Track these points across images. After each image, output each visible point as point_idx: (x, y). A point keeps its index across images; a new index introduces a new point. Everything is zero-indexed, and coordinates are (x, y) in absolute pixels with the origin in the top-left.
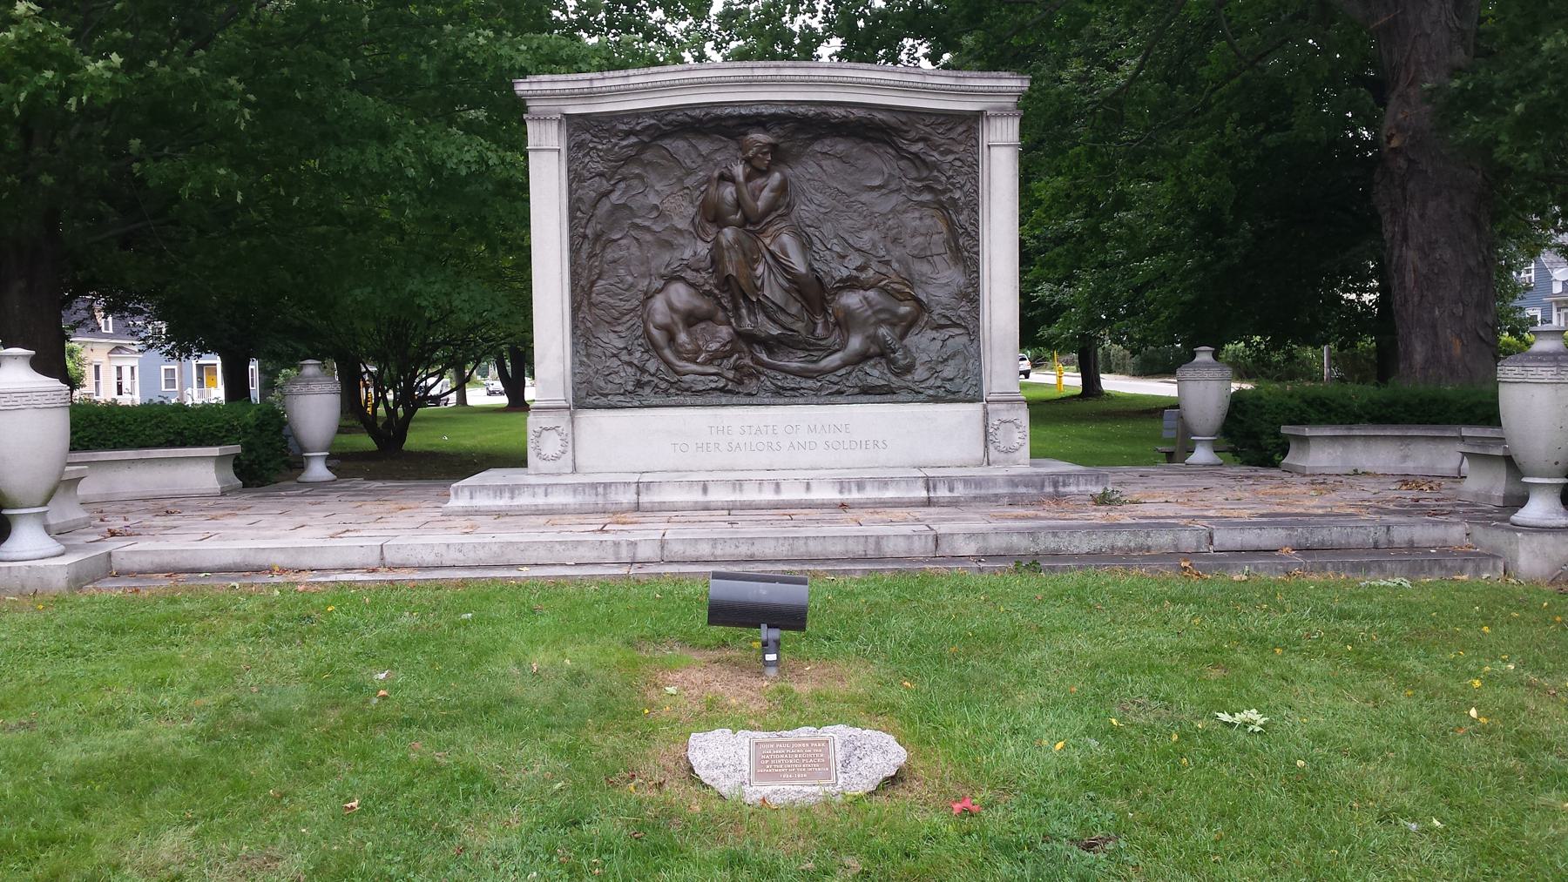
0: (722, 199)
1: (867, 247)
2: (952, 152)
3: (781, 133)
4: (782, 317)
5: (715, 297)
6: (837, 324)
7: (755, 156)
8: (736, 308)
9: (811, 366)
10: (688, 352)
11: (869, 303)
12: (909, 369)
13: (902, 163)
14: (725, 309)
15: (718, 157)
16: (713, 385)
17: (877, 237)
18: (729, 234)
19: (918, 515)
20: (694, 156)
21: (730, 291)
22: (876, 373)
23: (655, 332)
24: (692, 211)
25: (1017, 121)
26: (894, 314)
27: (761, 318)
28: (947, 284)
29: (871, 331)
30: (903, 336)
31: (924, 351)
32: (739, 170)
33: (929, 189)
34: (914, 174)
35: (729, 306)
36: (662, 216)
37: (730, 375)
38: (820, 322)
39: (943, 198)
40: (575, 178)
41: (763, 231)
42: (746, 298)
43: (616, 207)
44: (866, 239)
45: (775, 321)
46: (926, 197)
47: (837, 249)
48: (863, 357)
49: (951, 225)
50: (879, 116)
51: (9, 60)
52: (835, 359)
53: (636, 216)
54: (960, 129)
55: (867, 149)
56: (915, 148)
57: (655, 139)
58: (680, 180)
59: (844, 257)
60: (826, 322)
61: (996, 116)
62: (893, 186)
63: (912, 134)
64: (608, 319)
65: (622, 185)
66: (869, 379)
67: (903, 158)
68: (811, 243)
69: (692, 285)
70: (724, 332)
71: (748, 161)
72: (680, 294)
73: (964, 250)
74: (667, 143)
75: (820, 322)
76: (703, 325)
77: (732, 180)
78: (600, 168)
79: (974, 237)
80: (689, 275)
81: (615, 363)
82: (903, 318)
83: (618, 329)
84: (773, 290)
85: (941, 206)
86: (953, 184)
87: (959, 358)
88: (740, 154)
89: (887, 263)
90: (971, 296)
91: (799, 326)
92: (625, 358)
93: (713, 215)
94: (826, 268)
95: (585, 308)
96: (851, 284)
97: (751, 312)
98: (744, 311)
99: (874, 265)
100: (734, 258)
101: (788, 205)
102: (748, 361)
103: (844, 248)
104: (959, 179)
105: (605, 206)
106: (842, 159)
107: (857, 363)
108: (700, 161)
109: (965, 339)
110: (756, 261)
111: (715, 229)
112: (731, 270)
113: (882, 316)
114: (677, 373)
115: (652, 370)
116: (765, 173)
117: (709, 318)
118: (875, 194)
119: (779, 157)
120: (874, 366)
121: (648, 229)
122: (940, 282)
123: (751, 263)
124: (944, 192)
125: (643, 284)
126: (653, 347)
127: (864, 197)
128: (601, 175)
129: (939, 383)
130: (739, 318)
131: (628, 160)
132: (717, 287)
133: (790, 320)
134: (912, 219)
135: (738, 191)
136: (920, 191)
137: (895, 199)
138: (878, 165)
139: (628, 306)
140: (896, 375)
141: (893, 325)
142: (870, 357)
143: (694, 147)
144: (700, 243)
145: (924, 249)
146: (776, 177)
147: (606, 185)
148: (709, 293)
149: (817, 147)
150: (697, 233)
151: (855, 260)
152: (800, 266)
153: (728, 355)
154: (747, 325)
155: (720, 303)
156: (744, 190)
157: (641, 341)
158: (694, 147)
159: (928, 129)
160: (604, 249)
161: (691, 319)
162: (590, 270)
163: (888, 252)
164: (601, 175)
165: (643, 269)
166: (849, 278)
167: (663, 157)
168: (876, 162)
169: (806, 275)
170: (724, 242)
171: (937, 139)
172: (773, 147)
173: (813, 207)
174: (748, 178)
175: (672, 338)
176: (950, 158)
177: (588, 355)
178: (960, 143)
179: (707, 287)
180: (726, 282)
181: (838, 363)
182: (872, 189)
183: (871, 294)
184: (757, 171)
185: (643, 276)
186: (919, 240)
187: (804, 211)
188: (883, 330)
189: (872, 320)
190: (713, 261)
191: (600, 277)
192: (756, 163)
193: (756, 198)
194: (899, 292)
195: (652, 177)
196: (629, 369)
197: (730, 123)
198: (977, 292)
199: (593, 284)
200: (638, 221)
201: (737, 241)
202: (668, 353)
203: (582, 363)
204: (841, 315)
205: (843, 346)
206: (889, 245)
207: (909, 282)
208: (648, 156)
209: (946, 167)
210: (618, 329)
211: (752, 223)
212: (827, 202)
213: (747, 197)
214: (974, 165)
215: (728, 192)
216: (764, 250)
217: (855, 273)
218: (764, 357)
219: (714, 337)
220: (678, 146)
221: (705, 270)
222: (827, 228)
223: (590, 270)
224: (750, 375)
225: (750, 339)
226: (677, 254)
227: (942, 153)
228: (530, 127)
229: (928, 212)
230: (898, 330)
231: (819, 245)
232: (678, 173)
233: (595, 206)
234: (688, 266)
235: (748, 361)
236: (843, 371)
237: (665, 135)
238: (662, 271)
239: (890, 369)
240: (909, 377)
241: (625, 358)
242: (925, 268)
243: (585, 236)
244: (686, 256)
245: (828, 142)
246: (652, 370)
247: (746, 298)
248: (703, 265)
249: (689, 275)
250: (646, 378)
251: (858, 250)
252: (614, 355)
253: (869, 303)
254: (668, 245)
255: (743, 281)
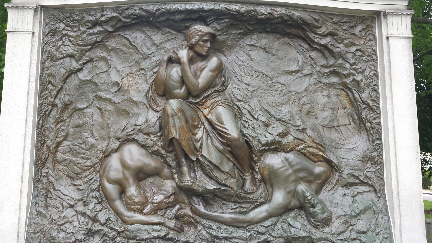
0: (169, 76)
1: (286, 118)
2: (354, 45)
3: (218, 27)
4: (218, 175)
5: (162, 156)
6: (263, 180)
7: (197, 43)
8: (179, 165)
9: (241, 217)
10: (135, 203)
11: (290, 163)
12: (327, 222)
13: (314, 54)
14: (169, 166)
15: (168, 45)
16: (156, 234)
17: (295, 110)
18: (174, 104)
19: (153, 77)
20: (149, 44)
21: (176, 151)
22: (298, 225)
23: (109, 186)
24: (146, 87)
25: (409, 19)
26: (311, 173)
27: (199, 174)
28: (353, 149)
29: (292, 187)
30: (318, 191)
31: (337, 205)
32: (184, 54)
33: (335, 73)
34: (323, 62)
35: (173, 164)
36: (120, 89)
37: (172, 224)
38: (248, 178)
39: (348, 81)
40: (47, 58)
41: (202, 103)
42: (187, 157)
43: (84, 83)
44: (284, 112)
45: (211, 178)
46: (334, 80)
47: (262, 119)
48: (286, 210)
49: (353, 102)
50: (297, 14)
51: (126, 137)
52: (261, 211)
53: (100, 91)
54: (359, 28)
55: (286, 43)
56: (324, 41)
57: (117, 30)
58: (138, 62)
59: (267, 126)
60: (253, 179)
61: (392, 14)
62: (307, 71)
63: (323, 30)
64: (71, 175)
65: (90, 65)
66: (292, 230)
67: (315, 49)
68: (241, 114)
69: (143, 146)
70: (169, 186)
71: (191, 47)
72: (134, 155)
73: (367, 120)
74: (128, 34)
75: (248, 178)
76: (151, 180)
77: (178, 61)
78: (71, 50)
79: (375, 110)
80: (141, 137)
81: (69, 213)
82: (318, 176)
83: (78, 182)
84: (210, 151)
85: (346, 87)
86: (355, 70)
87: (370, 213)
88: (185, 43)
89: (303, 131)
90: (375, 158)
91: (231, 182)
92: (80, 208)
93: (163, 90)
94: (254, 134)
95: (49, 164)
96: (274, 147)
97: (191, 169)
98: (185, 169)
99: (293, 131)
100: (178, 123)
101: (223, 84)
102: (187, 211)
103: (268, 119)
104: (360, 65)
105: (74, 81)
106: (265, 50)
107: (280, 215)
108: (154, 49)
109: (372, 195)
110: (196, 127)
111: (164, 102)
112: (175, 134)
113: (301, 175)
114: (125, 222)
115: (103, 221)
116: (205, 57)
117: (156, 173)
118: (291, 77)
119: (216, 45)
120: (295, 218)
121: (110, 101)
122: (351, 149)
123: (192, 128)
124: (347, 76)
125: (102, 145)
126: (105, 199)
127: (283, 79)
128: (71, 56)
129: (354, 235)
130: (181, 174)
131: (94, 45)
132: (163, 147)
133: (224, 176)
134: (321, 98)
135: (183, 70)
136: (328, 75)
137: (306, 82)
138: (293, 56)
139: (88, 163)
140: (316, 227)
141: (310, 182)
142: (291, 210)
143: (150, 38)
144: (151, 113)
145: (332, 121)
146: (213, 62)
147: (75, 65)
148: (156, 153)
149: (248, 41)
150: (150, 106)
151: (278, 128)
152: (233, 132)
153: (170, 206)
154: (188, 180)
155: (166, 162)
156: (187, 68)
157: (96, 193)
158: (150, 38)
159: (335, 26)
160: (71, 115)
161: (141, 175)
162: (57, 133)
163: (303, 122)
164: (71, 56)
165: (103, 132)
166: (273, 142)
167: (125, 45)
168: (293, 53)
169: (238, 140)
170: (169, 111)
171: (342, 34)
172: (213, 37)
173: (243, 86)
174: (191, 61)
175: (123, 191)
176: (354, 49)
177: (47, 206)
178: (360, 38)
179: (155, 148)
180: (171, 144)
181: (264, 214)
182: (290, 73)
183: (291, 156)
184: (198, 56)
185: (103, 138)
186: (327, 113)
187: (236, 89)
188: (302, 187)
189: (292, 178)
190: (161, 128)
191: (66, 138)
192: (198, 49)
193: (197, 76)
194: (313, 154)
195: (114, 60)
196: (82, 219)
197: (177, 17)
198: (380, 156)
199: (59, 144)
200: (101, 94)
201: (181, 110)
202: (119, 204)
203: (39, 214)
204: (266, 173)
205: (268, 200)
206: (305, 118)
207: (321, 146)
208: (112, 43)
209: (349, 56)
210: (78, 182)
211: (194, 96)
212: (254, 82)
213: (190, 75)
214: (372, 57)
215: (175, 72)
216: (203, 119)
217: (278, 138)
218: (201, 208)
219: (160, 189)
220: (137, 37)
221: (154, 134)
222: (254, 103)
223: (57, 133)
224: (189, 224)
225: (190, 192)
226: (132, 121)
227: (346, 45)
228: (11, 14)
229: (333, 91)
230: (314, 187)
231: (248, 116)
232: (136, 58)
233: (65, 81)
234: (140, 131)
235: (187, 211)
236: (269, 223)
237: (127, 27)
238: (119, 134)
239: (309, 221)
240: (327, 229)
241: (80, 208)
242: (334, 135)
243: (54, 105)
244: (139, 123)
245: (255, 36)
246: (103, 221)
247: (187, 157)
248: (152, 130)
249: (141, 137)
250: (96, 227)
251: (279, 120)
252: (71, 206)
253: (290, 163)
254: (126, 113)
255: (184, 143)
